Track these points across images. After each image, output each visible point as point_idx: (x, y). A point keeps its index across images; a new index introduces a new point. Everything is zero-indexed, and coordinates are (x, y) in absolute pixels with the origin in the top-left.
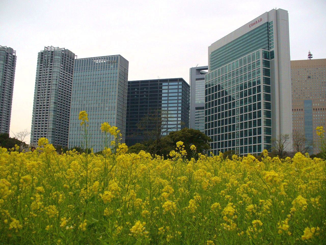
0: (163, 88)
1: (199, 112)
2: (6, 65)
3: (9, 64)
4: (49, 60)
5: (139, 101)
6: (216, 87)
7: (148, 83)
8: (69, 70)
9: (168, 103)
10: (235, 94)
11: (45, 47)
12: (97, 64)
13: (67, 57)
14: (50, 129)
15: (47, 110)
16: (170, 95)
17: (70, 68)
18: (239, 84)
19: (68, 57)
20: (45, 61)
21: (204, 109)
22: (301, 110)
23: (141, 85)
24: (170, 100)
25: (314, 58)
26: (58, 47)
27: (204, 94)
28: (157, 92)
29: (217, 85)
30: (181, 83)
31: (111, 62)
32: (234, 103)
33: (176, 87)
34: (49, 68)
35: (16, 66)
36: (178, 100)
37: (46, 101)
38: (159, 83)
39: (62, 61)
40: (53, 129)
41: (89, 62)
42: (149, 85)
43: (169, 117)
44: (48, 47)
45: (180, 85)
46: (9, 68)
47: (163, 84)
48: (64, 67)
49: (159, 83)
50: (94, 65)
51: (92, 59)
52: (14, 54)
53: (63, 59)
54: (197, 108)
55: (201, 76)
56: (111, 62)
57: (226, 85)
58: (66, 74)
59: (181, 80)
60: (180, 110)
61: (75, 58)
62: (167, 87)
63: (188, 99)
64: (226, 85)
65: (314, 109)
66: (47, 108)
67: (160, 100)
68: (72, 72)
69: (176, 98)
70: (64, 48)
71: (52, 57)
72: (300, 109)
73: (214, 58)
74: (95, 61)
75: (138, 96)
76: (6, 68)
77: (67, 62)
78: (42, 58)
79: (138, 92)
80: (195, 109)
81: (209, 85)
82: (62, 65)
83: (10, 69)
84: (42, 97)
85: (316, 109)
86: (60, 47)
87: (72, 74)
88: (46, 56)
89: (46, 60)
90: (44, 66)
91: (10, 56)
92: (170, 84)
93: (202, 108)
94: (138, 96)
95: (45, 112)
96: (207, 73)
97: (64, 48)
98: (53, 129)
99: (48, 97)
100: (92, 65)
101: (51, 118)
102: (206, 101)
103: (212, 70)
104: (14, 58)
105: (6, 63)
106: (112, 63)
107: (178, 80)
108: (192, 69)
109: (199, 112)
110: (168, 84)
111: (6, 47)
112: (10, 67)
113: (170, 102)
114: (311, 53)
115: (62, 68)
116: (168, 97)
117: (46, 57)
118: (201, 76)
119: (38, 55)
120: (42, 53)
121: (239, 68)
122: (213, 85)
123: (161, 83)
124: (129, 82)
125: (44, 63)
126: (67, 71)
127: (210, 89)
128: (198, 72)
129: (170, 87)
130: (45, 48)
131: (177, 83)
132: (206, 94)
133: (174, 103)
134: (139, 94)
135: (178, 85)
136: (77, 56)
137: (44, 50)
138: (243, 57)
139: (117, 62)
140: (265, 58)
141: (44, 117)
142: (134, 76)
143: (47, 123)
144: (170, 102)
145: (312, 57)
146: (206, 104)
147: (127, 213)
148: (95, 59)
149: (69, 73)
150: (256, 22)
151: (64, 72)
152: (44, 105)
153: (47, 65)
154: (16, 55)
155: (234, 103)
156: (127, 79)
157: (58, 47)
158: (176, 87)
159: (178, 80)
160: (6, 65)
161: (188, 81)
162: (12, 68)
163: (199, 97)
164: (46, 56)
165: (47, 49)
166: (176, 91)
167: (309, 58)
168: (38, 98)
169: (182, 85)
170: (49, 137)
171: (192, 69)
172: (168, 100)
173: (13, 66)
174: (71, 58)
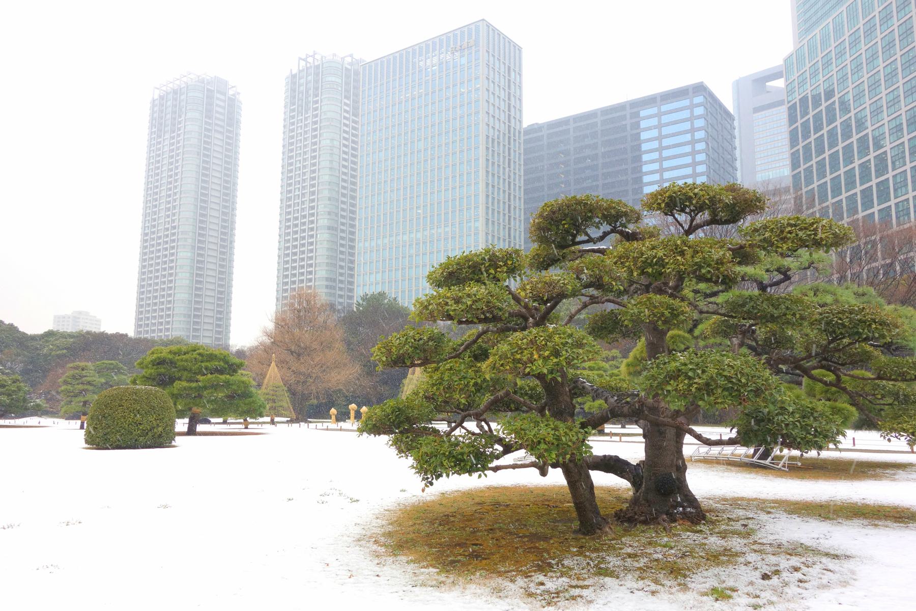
3: (216, 118)
4: (311, 92)
11: (300, 59)
24: (669, 158)
30: (699, 99)
33: (686, 114)
40: (327, 279)
47: (643, 113)
69: (688, 149)
71: (316, 82)
73: (810, 18)
78: (293, 90)
92: (664, 108)
97: (351, 56)
98: (327, 279)
102: (795, 164)
104: (232, 105)
112: (223, 127)
113: (666, 164)
120: (293, 76)
123: (635, 110)
129: (665, 119)
131: (686, 103)
133: (673, 135)
135: (692, 107)
147: (181, 415)
164: (302, 81)
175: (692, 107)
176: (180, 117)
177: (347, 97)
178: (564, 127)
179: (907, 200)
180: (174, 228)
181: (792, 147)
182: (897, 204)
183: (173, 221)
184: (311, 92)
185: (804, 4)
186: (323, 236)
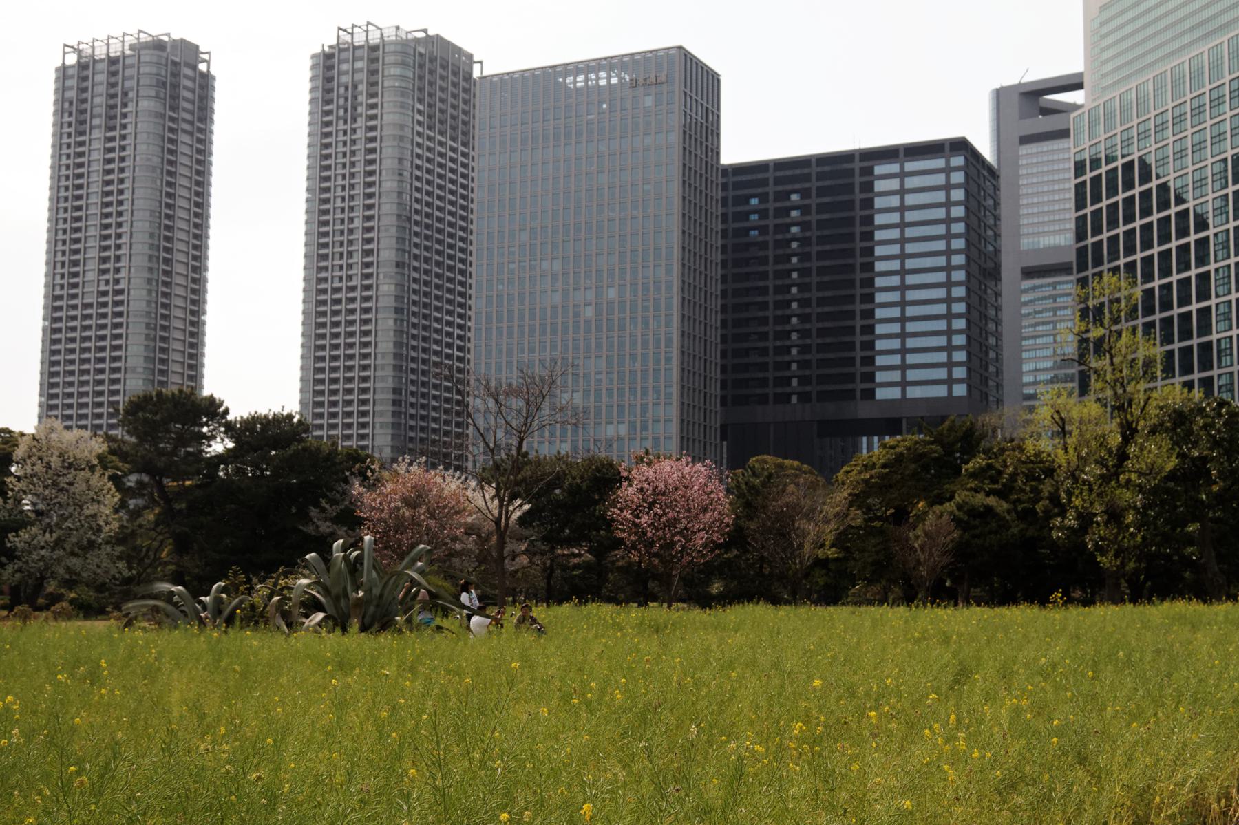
0: (879, 186)
2: (172, 119)
3: (185, 110)
4: (362, 88)
5: (771, 253)
6: (1128, 167)
7: (806, 171)
8: (454, 128)
9: (903, 256)
10: (1206, 200)
13: (439, 70)
14: (383, 367)
15: (367, 310)
16: (911, 216)
17: (454, 118)
19: (444, 67)
20: (342, 90)
21: (1071, 274)
23: (778, 181)
26: (398, 28)
27: (1072, 205)
28: (776, 193)
29: (1135, 157)
30: (958, 161)
31: (641, 81)
32: (1203, 244)
33: (940, 179)
35: (217, 117)
36: (948, 237)
37: (356, 270)
38: (857, 165)
39: (421, 90)
41: (542, 85)
42: (814, 177)
44: (354, 26)
45: (957, 169)
46: (184, 131)
47: (879, 170)
48: (430, 117)
49: (857, 165)
51: (559, 74)
52: (202, 67)
53: (421, 78)
54: (1029, 273)
55: (1043, 124)
56: (641, 81)
57: (1180, 154)
58: (441, 144)
59: (961, 146)
61: (476, 73)
62: (894, 184)
63: (990, 233)
64: (1180, 154)
66: (367, 299)
70: (425, 31)
71: (373, 72)
74: (570, 79)
75: (763, 230)
76: (171, 130)
77: (442, 89)
78: (329, 80)
79: (763, 214)
80: (1018, 274)
81: (1095, 163)
82: (421, 107)
83: (191, 134)
84: (342, 254)
86: (407, 26)
88: (344, 67)
89: (347, 88)
90: (341, 112)
91: (186, 77)
92: (910, 166)
93: (1064, 269)
94: (763, 230)
95: (357, 317)
96: (1076, 107)
97: (425, 31)
99: (368, 253)
101: (385, 344)
102: (1080, 235)
104: (206, 82)
105: (173, 109)
107: (947, 148)
108: (1000, 95)
110: (902, 167)
111: (166, 38)
112: (192, 123)
115: (421, 118)
117: (346, 73)
118: (1043, 124)
119: (309, 63)
122: (1114, 159)
125: (342, 101)
126: (454, 139)
127: (1096, 180)
128: (1032, 108)
129: (911, 182)
130: (341, 33)
131: (939, 163)
132: (1080, 204)
134: (771, 222)
135: (948, 170)
136: (481, 62)
137: (334, 42)
141: (356, 340)
142: (751, 134)
143: (368, 389)
146: (1081, 252)
148: (559, 74)
149: (441, 133)
152: (353, 289)
154: (213, 72)
155: (1203, 244)
156: (718, 154)
157: (398, 28)
158: (940, 179)
159: (947, 148)
160: (172, 119)
161: (985, 148)
162: (200, 130)
163: (1042, 218)
164: (344, 67)
165: (348, 38)
168: (324, 257)
169: (965, 169)
170: (383, 369)
172: (903, 241)
173: (201, 120)
174: (455, 74)
175: (948, 170)
176: (125, 105)
177: (420, 101)
178: (760, 176)
179: (1229, 266)
180: (120, 292)
181: (1078, 209)
182: (1226, 186)
183: (117, 281)
184: (362, 88)
185: (1103, 8)
186: (386, 324)
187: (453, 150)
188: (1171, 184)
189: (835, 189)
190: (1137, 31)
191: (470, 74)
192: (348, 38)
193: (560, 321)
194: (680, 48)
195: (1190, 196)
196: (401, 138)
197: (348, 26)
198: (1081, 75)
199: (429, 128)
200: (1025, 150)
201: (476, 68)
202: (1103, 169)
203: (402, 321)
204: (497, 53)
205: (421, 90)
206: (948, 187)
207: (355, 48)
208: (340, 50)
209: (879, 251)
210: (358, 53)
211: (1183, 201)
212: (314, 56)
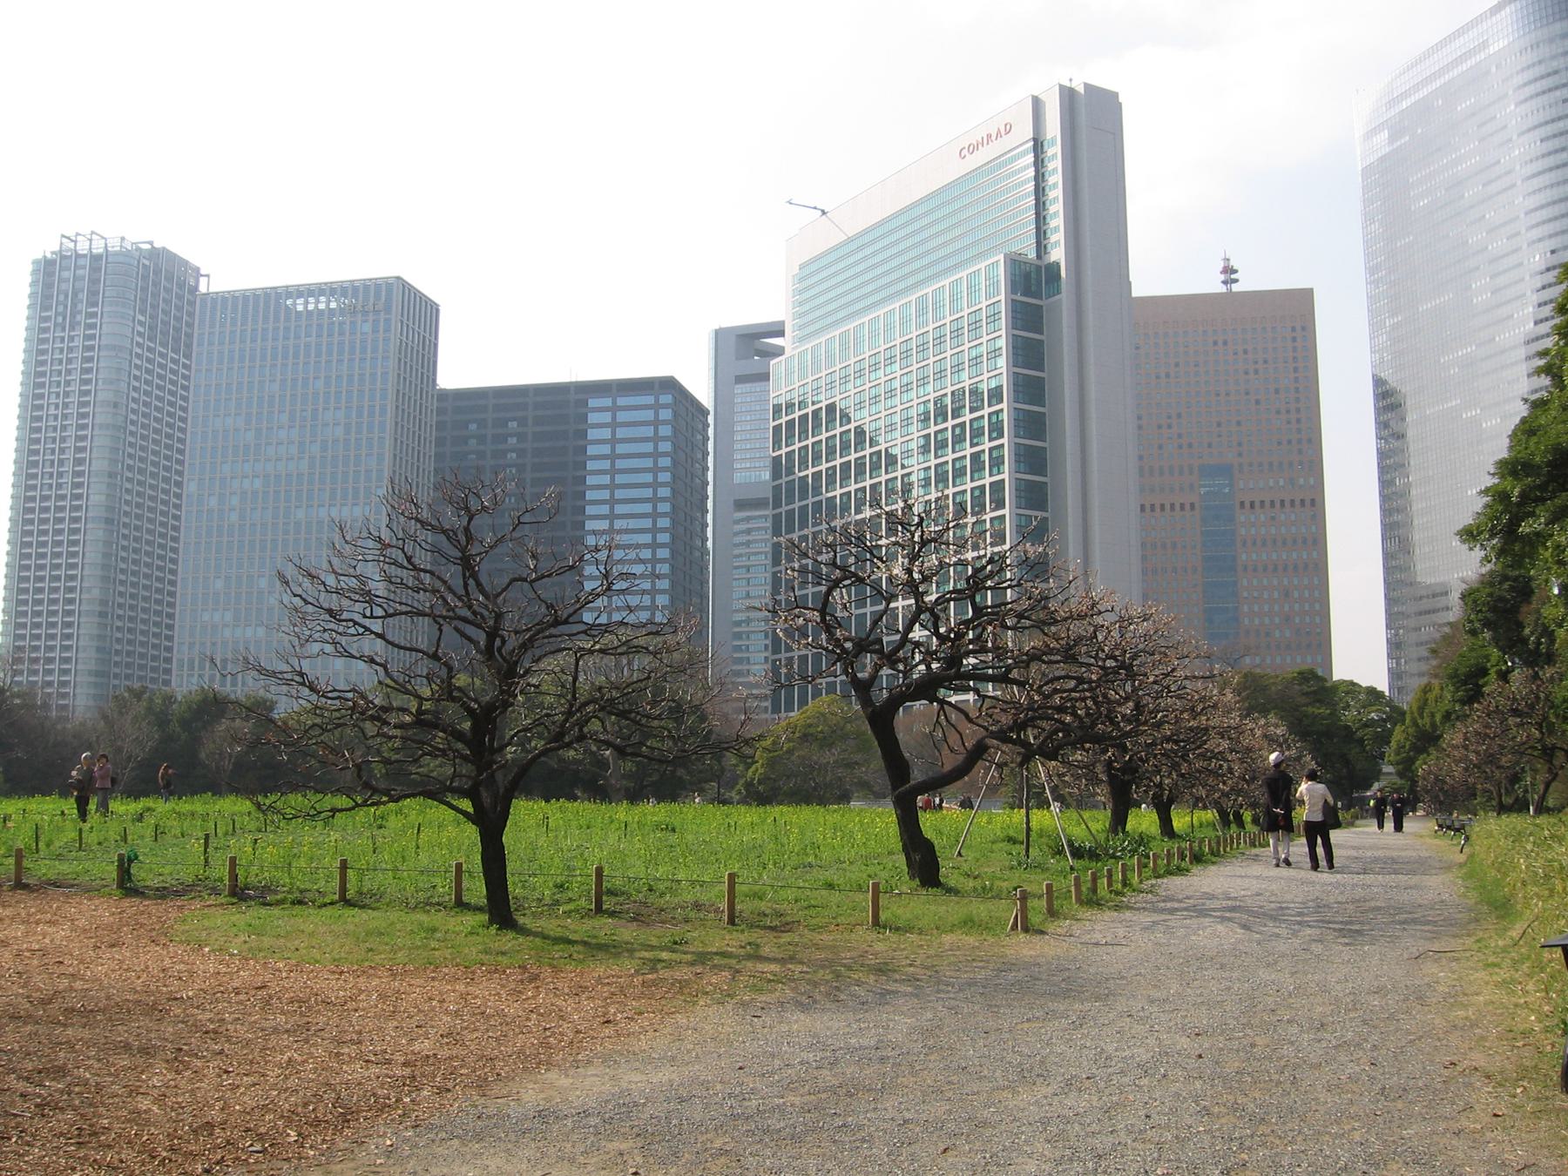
0: (593, 418)
1: (748, 519)
4: (84, 296)
12: (298, 314)
16: (621, 449)
18: (949, 390)
20: (62, 298)
22: (1188, 507)
24: (645, 440)
25: (1247, 283)
29: (823, 405)
30: (666, 399)
31: (359, 307)
33: (648, 415)
34: (80, 331)
43: (619, 532)
45: (665, 406)
47: (592, 403)
50: (287, 319)
51: (278, 295)
54: (741, 505)
56: (359, 307)
58: (161, 355)
60: (664, 515)
61: (203, 288)
62: (606, 417)
65: (1242, 503)
67: (579, 473)
68: (189, 346)
72: (1162, 506)
74: (289, 302)
85: (1252, 505)
87: (188, 356)
88: (65, 274)
90: (60, 319)
92: (621, 401)
93: (759, 503)
99: (79, 462)
100: (277, 320)
102: (776, 474)
103: (801, 340)
106: (365, 313)
108: (720, 335)
109: (748, 519)
114: (1234, 264)
116: (613, 457)
119: (30, 268)
121: (966, 311)
123: (580, 396)
124: (445, 395)
125: (61, 309)
126: (164, 345)
128: (747, 350)
129: (622, 416)
131: (650, 400)
133: (636, 408)
137: (57, 248)
138: (929, 290)
139: (388, 310)
140: (1025, 294)
142: (462, 367)
144: (619, 479)
145: (1236, 281)
146: (777, 489)
150: (989, 136)
151: (150, 349)
152: (63, 497)
153: (73, 315)
156: (434, 380)
157: (123, 239)
164: (65, 274)
165: (72, 245)
166: (648, 431)
167: (1225, 282)
168: (35, 464)
171: (720, 335)
175: (657, 407)
177: (143, 312)
186: (95, 534)
187: (174, 361)
188: (866, 428)
189: (552, 419)
190: (945, 244)
191: (196, 288)
192: (72, 245)
193: (269, 538)
194: (398, 278)
195: (881, 439)
196: (116, 405)
197: (71, 234)
198: (783, 323)
199: (150, 339)
200: (739, 389)
201: (203, 281)
202: (797, 415)
203: (116, 461)
204: (226, 270)
205: (144, 301)
206: (656, 423)
207: (78, 256)
208: (63, 257)
209: (590, 480)
210: (81, 262)
211: (878, 444)
212: (36, 262)
